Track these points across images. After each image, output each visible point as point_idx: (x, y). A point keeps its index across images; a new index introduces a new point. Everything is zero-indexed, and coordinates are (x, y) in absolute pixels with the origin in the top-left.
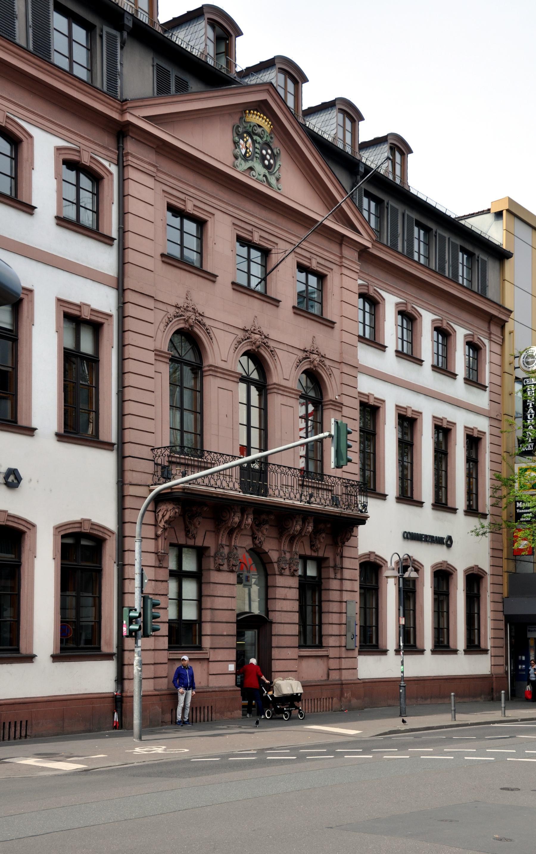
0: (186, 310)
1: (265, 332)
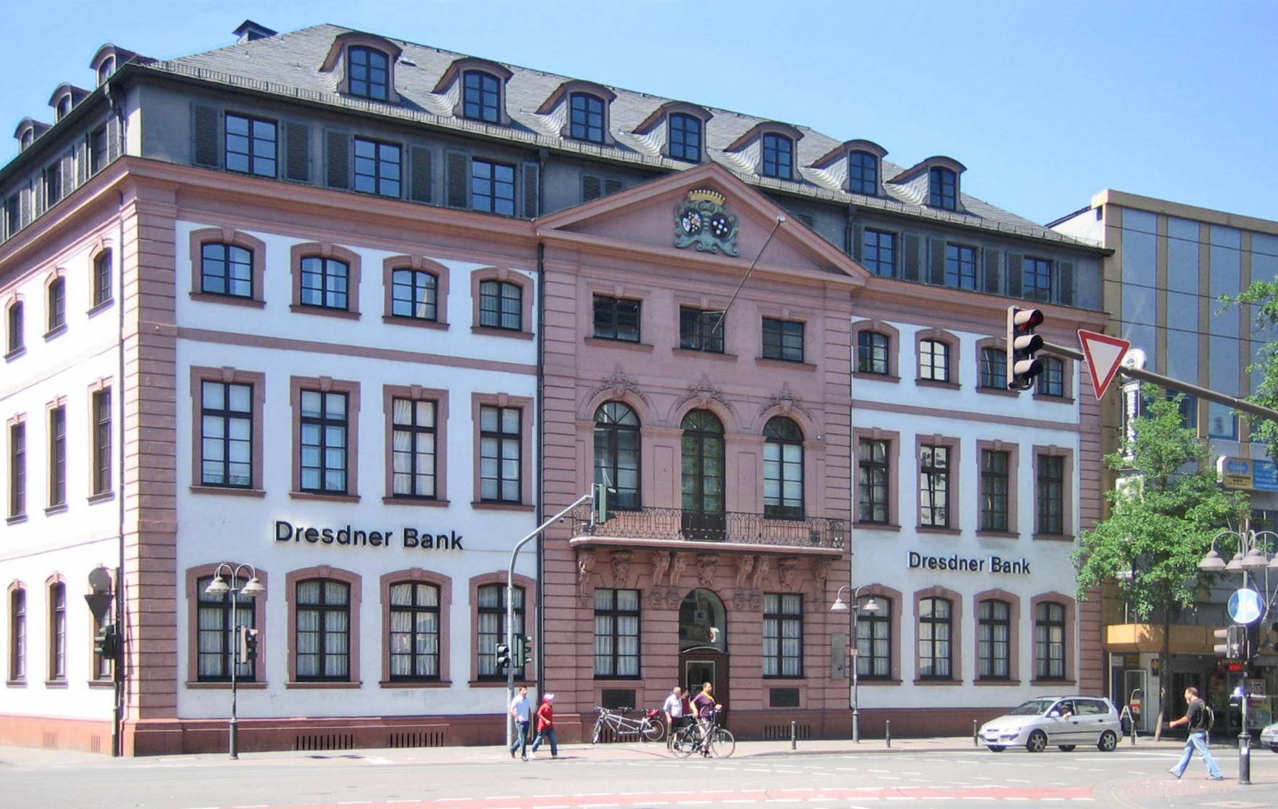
0: (615, 382)
1: (716, 387)
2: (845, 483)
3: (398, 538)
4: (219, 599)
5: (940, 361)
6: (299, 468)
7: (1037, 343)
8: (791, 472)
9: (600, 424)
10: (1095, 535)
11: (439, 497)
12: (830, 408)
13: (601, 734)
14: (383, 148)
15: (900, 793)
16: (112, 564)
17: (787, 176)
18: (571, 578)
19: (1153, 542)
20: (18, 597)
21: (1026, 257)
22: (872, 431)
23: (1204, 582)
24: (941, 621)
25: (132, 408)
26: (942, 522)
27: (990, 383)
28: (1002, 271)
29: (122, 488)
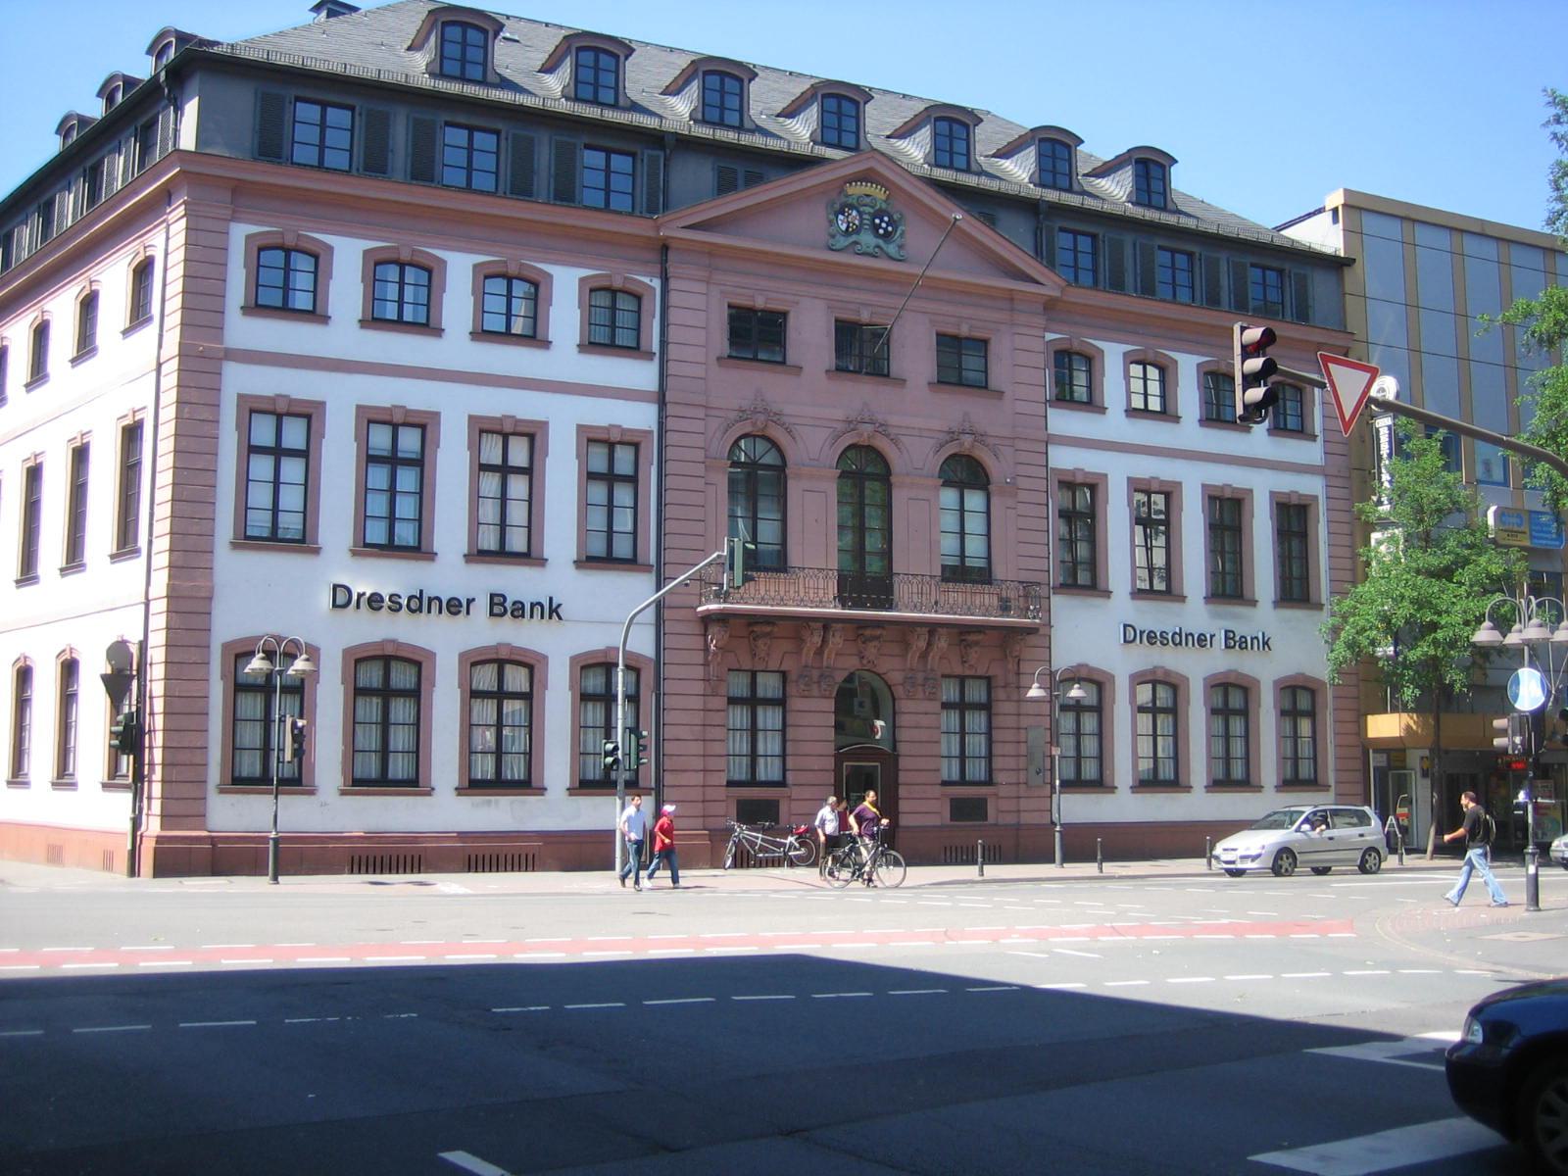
0: (755, 412)
1: (880, 418)
2: (1041, 537)
3: (482, 606)
4: (261, 681)
5: (1154, 387)
6: (362, 518)
7: (1270, 367)
8: (975, 524)
9: (735, 464)
10: (1348, 603)
11: (534, 554)
12: (1021, 445)
13: (735, 857)
14: (477, 135)
15: (1116, 931)
16: (134, 636)
17: (964, 167)
18: (699, 657)
19: (1418, 610)
20: (24, 676)
21: (1253, 265)
22: (1074, 472)
23: (1480, 661)
24: (1164, 711)
25: (167, 445)
26: (1162, 587)
27: (1216, 415)
28: (1224, 282)
29: (150, 542)
